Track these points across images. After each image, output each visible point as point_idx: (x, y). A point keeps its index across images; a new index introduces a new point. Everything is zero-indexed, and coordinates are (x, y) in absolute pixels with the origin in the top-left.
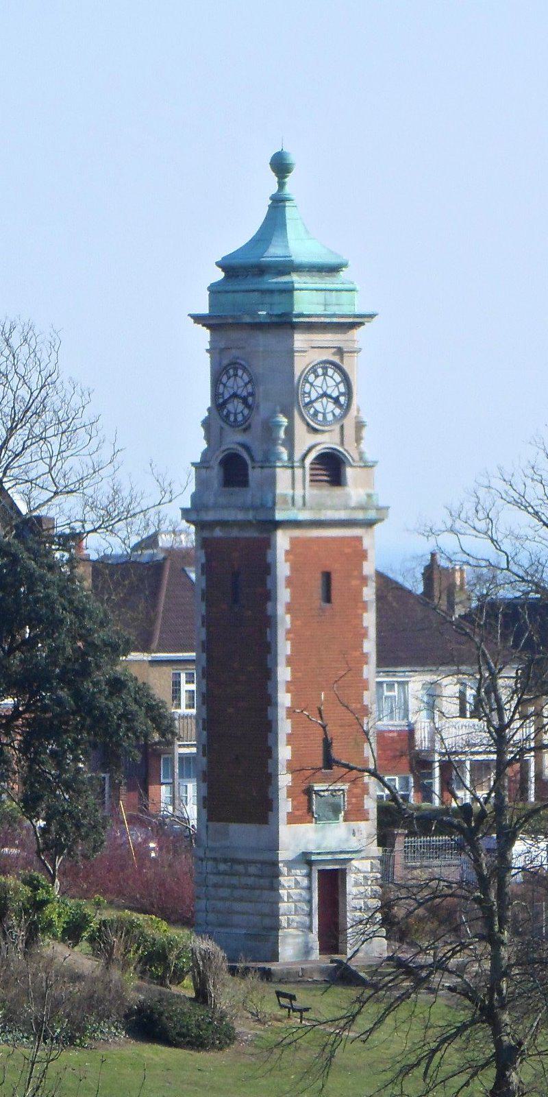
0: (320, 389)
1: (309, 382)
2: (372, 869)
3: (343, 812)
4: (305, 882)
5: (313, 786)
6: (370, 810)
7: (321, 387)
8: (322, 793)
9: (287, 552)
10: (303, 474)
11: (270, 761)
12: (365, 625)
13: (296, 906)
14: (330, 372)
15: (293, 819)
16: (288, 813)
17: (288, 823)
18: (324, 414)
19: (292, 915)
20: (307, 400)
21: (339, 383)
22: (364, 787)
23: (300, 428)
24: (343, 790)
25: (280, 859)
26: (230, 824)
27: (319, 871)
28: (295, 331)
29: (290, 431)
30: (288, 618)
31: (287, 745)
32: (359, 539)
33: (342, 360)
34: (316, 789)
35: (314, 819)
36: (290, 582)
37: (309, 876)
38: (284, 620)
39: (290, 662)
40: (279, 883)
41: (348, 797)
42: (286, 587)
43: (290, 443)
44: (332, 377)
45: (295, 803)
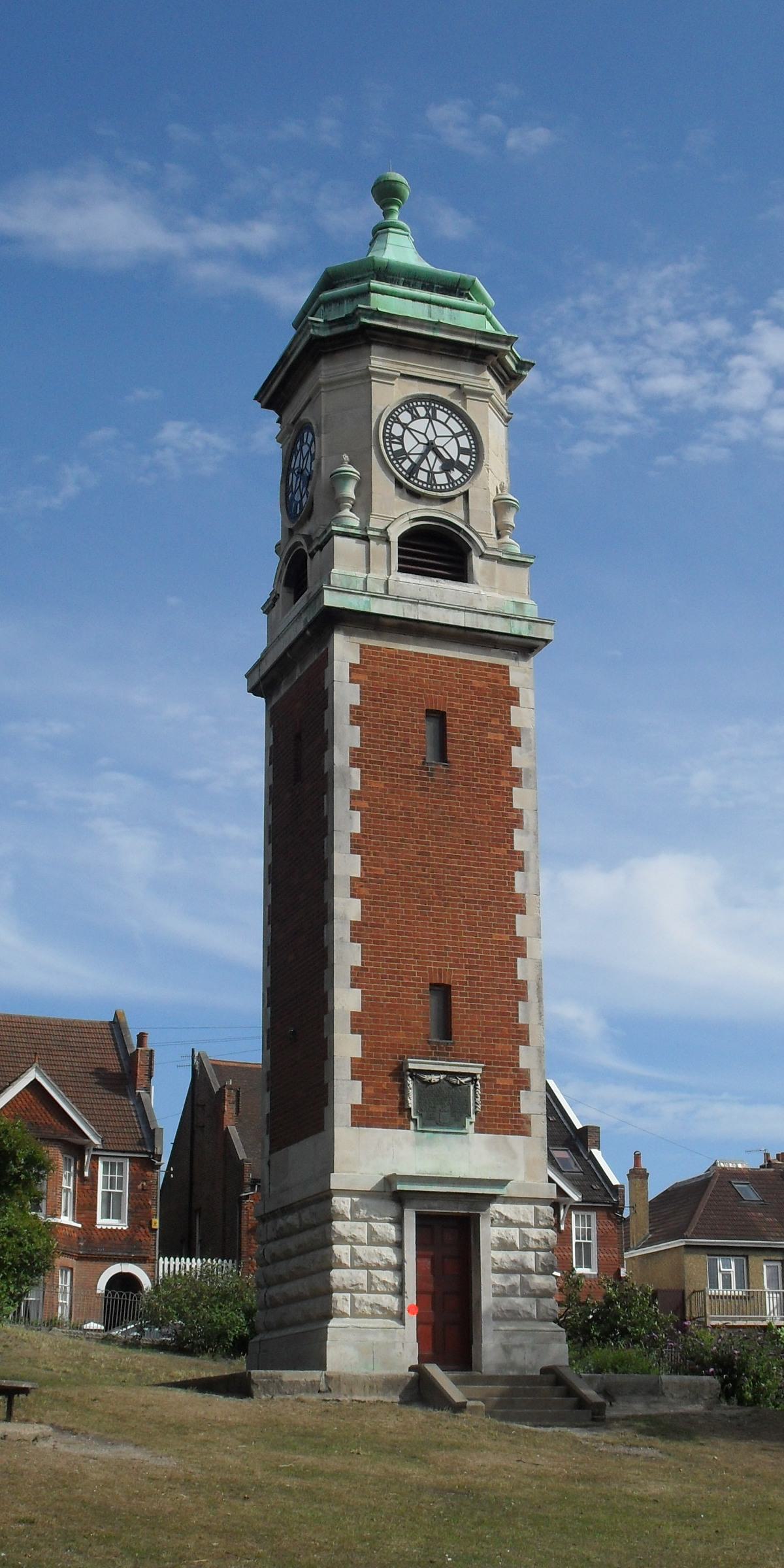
0: (423, 436)
1: (399, 422)
2: (536, 1220)
3: (473, 1116)
4: (391, 1231)
5: (408, 1062)
6: (533, 1118)
7: (425, 434)
8: (427, 1078)
9: (353, 668)
10: (386, 556)
11: (269, 985)
12: (516, 805)
13: (370, 1277)
14: (441, 415)
15: (362, 1118)
16: (353, 1106)
17: (353, 1125)
18: (405, 426)
19: (363, 1292)
20: (407, 465)
21: (460, 434)
22: (519, 1076)
23: (382, 485)
24: (473, 1075)
25: (334, 1185)
26: (288, 1148)
27: (35, 1081)
28: (374, 348)
29: (364, 486)
30: (356, 773)
31: (353, 986)
32: (505, 670)
33: (465, 405)
34: (411, 1066)
35: (412, 1124)
36: (357, 715)
37: (399, 1222)
38: (346, 777)
39: (357, 846)
40: (331, 1231)
41: (483, 1091)
42: (352, 723)
43: (364, 504)
44: (445, 424)
45: (370, 1090)
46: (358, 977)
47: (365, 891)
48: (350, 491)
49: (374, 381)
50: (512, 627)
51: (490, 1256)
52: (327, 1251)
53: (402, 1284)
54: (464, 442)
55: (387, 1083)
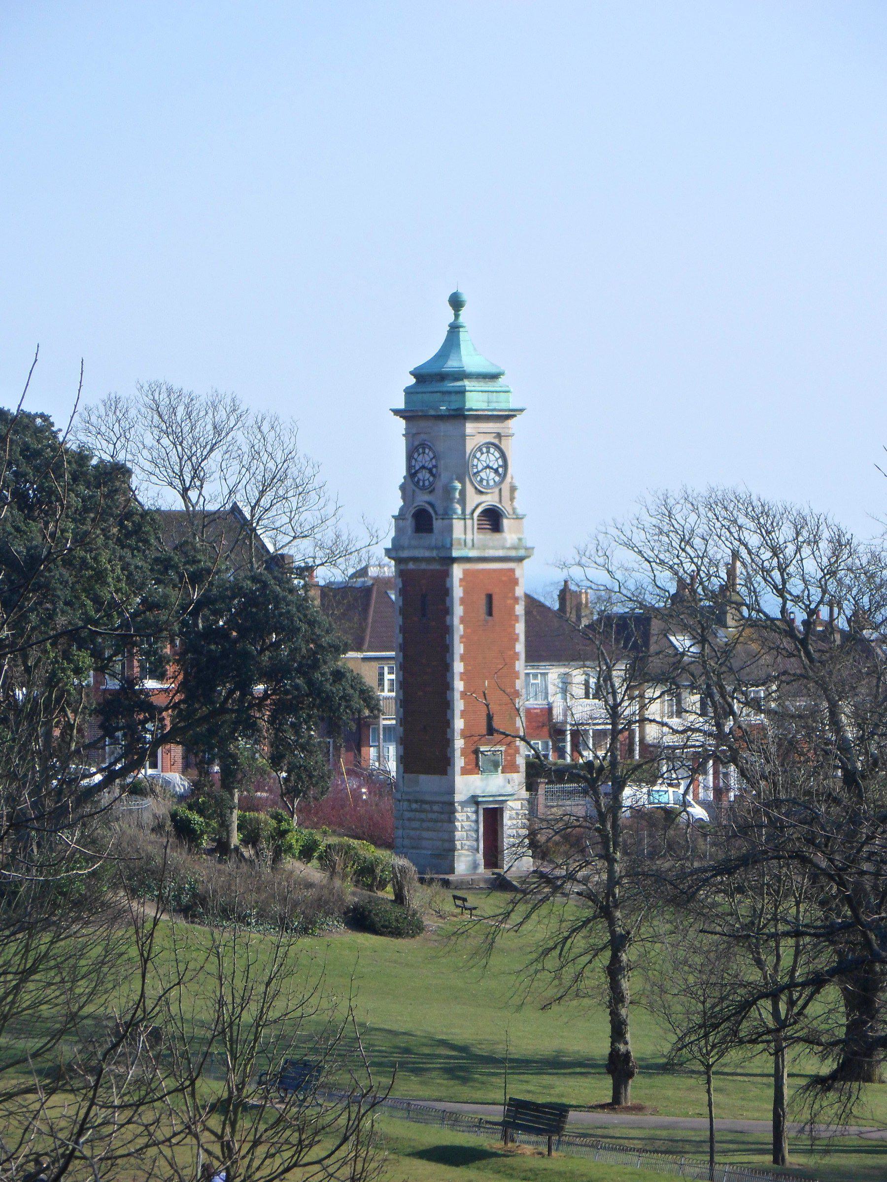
4: (474, 817)
9: (461, 580)
14: (492, 450)
15: (465, 772)
20: (475, 470)
29: (463, 493)
32: (512, 571)
36: (463, 601)
37: (476, 812)
38: (458, 628)
39: (463, 658)
43: (463, 501)
46: (463, 714)
47: (464, 677)
48: (457, 495)
49: (769, 1144)
50: (129, 1149)
51: (507, 822)
52: (451, 853)
53: (478, 827)
54: (500, 462)
55: (473, 756)
